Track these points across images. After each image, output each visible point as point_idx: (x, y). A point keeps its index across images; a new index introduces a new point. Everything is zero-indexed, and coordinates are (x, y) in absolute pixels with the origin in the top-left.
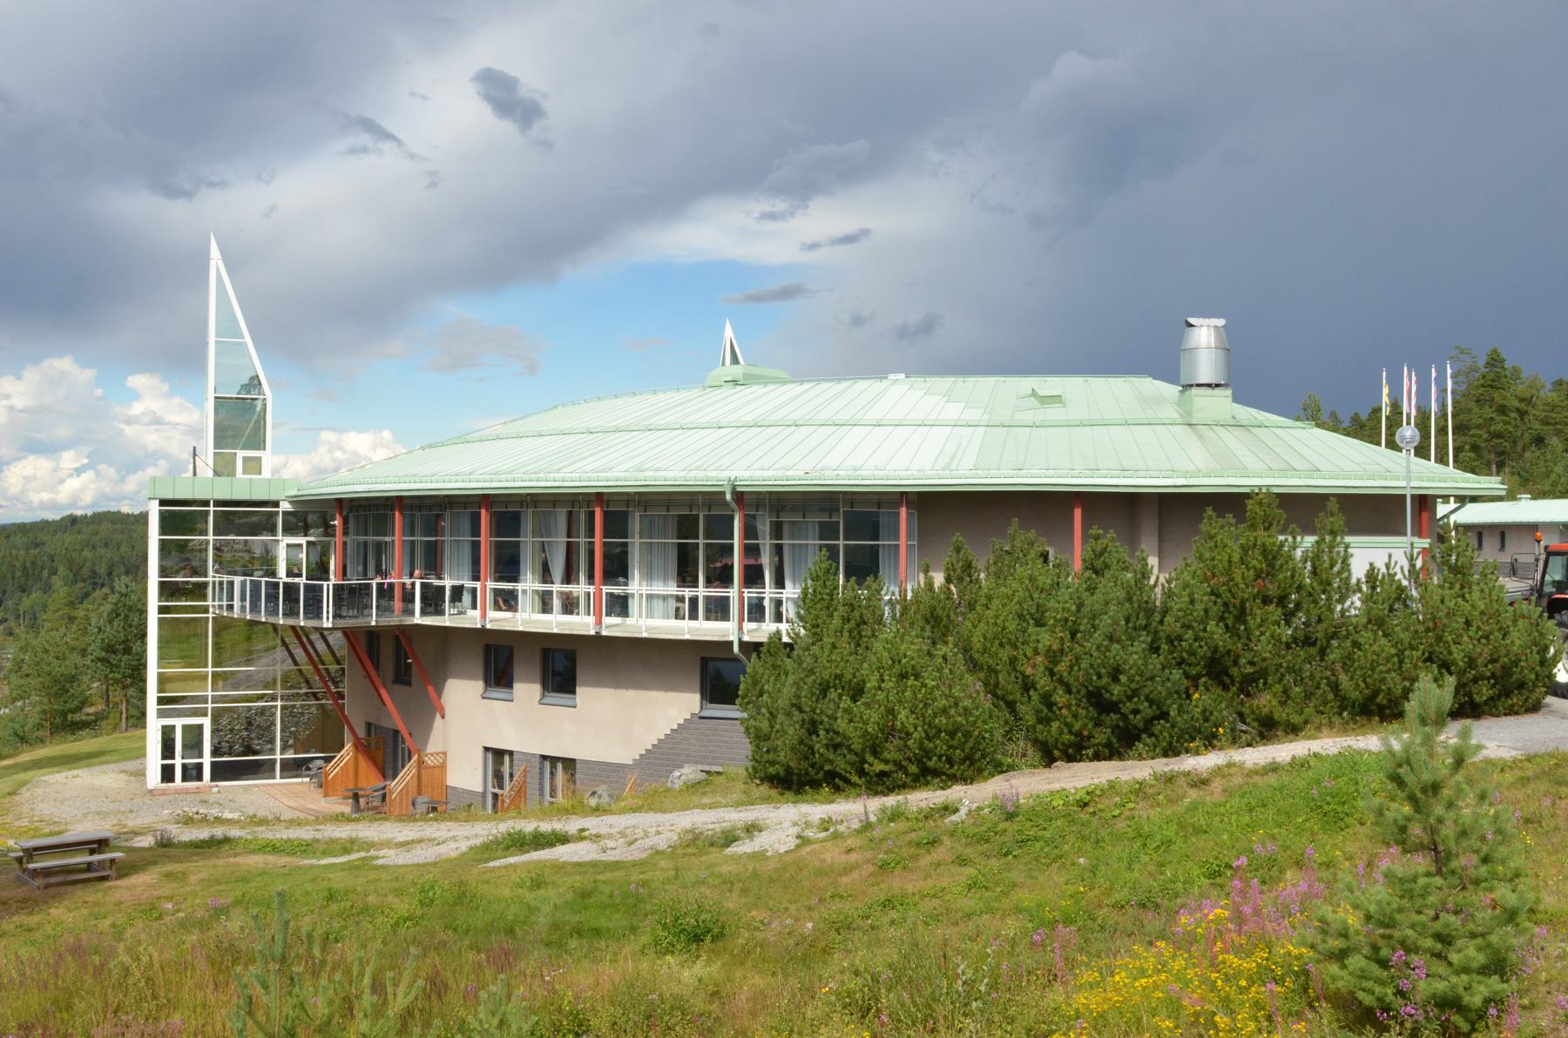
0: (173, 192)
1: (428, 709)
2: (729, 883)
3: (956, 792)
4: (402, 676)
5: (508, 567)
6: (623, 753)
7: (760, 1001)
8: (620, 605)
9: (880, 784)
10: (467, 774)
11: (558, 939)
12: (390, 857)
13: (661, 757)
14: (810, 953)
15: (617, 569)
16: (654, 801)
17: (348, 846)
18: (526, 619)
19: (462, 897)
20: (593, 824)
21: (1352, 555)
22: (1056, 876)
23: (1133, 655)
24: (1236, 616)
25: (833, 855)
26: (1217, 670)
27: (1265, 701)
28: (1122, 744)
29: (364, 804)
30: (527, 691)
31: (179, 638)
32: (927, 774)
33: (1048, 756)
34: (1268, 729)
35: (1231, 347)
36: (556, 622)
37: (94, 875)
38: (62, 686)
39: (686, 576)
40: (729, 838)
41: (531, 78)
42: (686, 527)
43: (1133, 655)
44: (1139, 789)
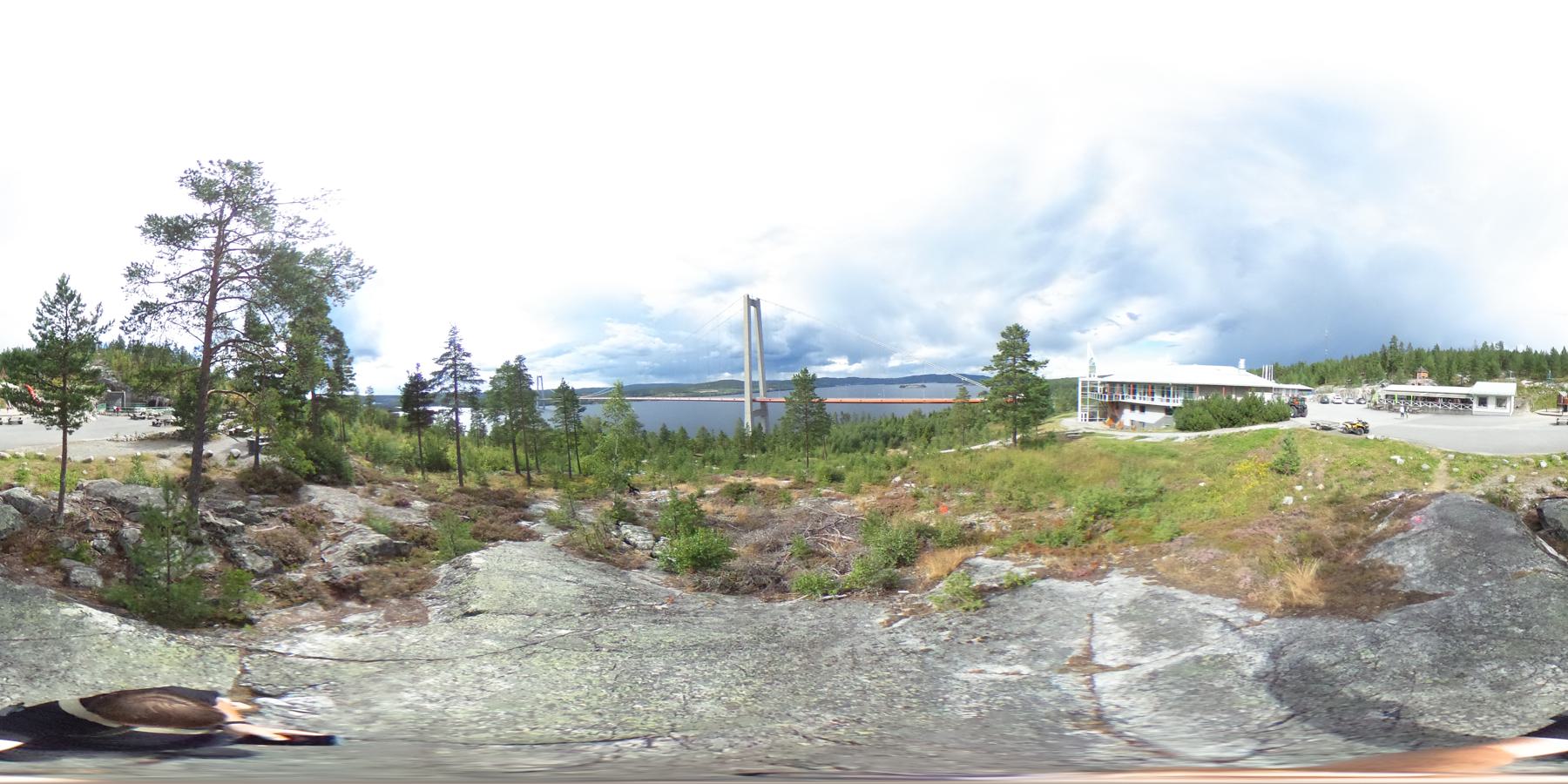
0: (1083, 332)
1: (1121, 413)
2: (1176, 447)
3: (1208, 433)
4: (1117, 408)
5: (1134, 393)
6: (1153, 422)
7: (1185, 467)
8: (1134, 398)
9: (1196, 430)
10: (1127, 423)
11: (1151, 455)
12: (1120, 438)
13: (1159, 423)
14: (1190, 460)
15: (1153, 394)
16: (1159, 431)
17: (1112, 436)
18: (1137, 401)
19: (1134, 447)
20: (1152, 435)
21: (370, 389)
22: (1226, 447)
23: (1235, 413)
24: (1250, 407)
25: (1191, 443)
26: (1247, 415)
27: (1254, 419)
28: (1233, 425)
29: (1112, 427)
30: (1137, 412)
31: (1084, 401)
32: (1204, 429)
33: (1222, 427)
34: (1254, 424)
35: (1246, 364)
36: (1142, 402)
37: (1073, 438)
38: (1064, 405)
39: (1163, 396)
40: (1173, 439)
41: (1136, 312)
42: (1163, 388)
43: (1235, 413)
44: (1237, 434)
